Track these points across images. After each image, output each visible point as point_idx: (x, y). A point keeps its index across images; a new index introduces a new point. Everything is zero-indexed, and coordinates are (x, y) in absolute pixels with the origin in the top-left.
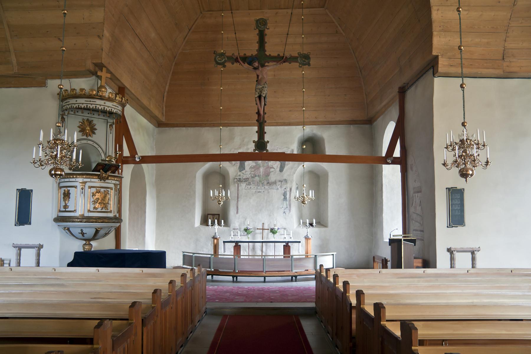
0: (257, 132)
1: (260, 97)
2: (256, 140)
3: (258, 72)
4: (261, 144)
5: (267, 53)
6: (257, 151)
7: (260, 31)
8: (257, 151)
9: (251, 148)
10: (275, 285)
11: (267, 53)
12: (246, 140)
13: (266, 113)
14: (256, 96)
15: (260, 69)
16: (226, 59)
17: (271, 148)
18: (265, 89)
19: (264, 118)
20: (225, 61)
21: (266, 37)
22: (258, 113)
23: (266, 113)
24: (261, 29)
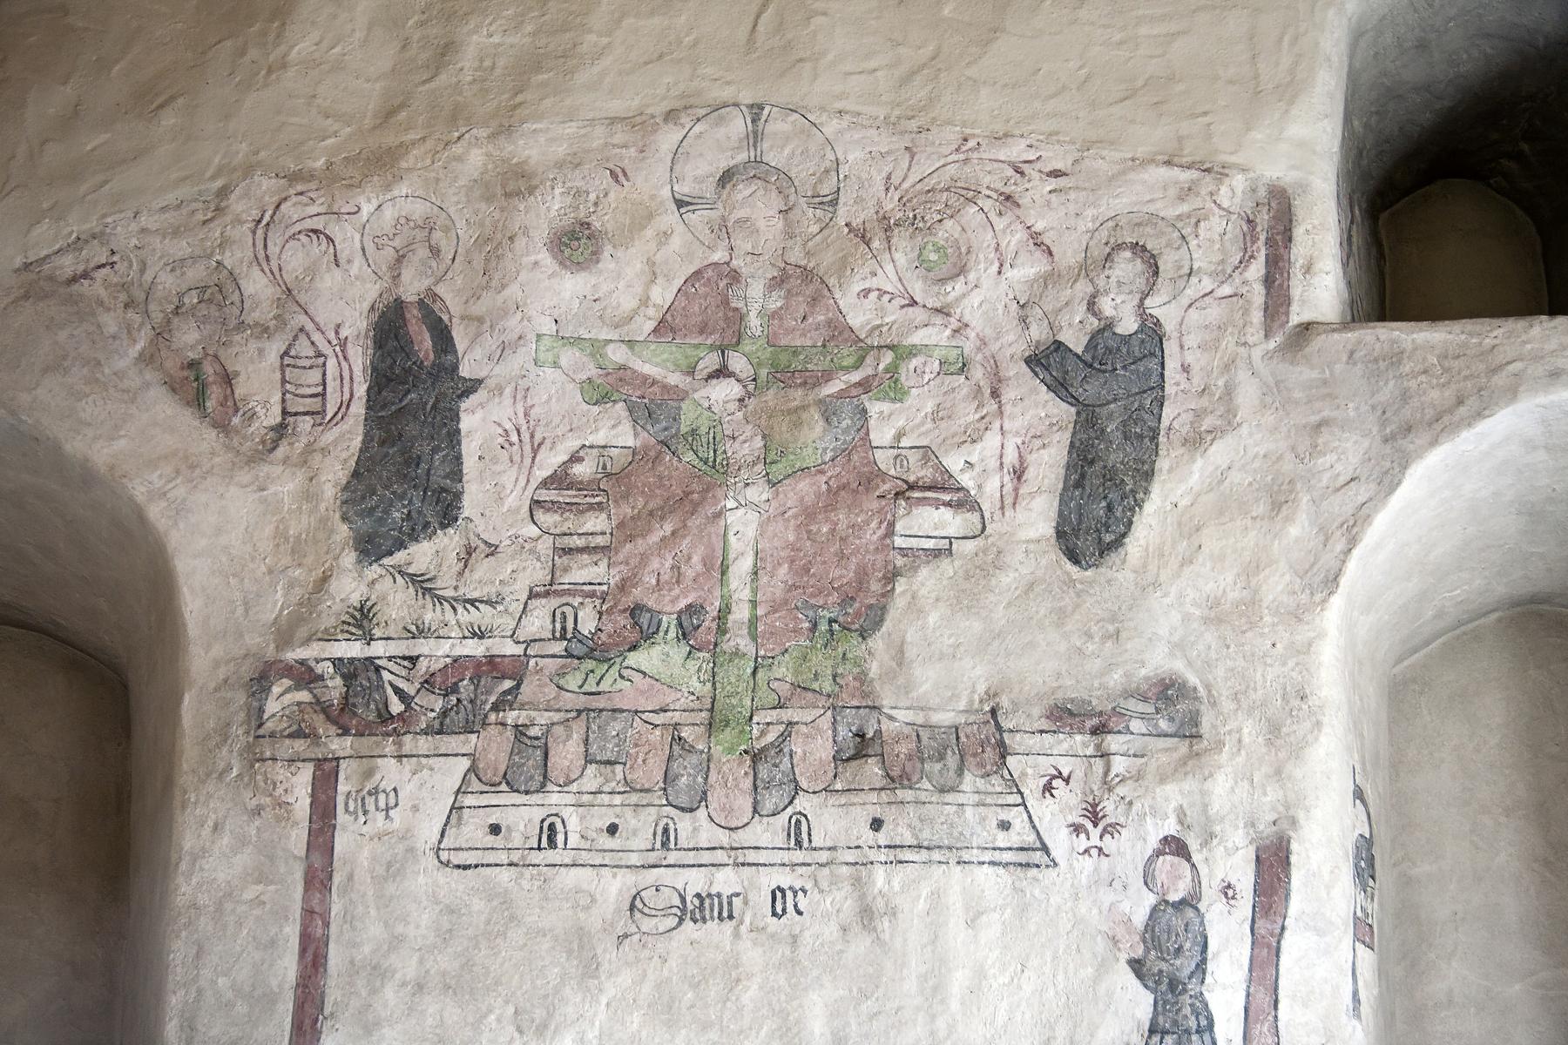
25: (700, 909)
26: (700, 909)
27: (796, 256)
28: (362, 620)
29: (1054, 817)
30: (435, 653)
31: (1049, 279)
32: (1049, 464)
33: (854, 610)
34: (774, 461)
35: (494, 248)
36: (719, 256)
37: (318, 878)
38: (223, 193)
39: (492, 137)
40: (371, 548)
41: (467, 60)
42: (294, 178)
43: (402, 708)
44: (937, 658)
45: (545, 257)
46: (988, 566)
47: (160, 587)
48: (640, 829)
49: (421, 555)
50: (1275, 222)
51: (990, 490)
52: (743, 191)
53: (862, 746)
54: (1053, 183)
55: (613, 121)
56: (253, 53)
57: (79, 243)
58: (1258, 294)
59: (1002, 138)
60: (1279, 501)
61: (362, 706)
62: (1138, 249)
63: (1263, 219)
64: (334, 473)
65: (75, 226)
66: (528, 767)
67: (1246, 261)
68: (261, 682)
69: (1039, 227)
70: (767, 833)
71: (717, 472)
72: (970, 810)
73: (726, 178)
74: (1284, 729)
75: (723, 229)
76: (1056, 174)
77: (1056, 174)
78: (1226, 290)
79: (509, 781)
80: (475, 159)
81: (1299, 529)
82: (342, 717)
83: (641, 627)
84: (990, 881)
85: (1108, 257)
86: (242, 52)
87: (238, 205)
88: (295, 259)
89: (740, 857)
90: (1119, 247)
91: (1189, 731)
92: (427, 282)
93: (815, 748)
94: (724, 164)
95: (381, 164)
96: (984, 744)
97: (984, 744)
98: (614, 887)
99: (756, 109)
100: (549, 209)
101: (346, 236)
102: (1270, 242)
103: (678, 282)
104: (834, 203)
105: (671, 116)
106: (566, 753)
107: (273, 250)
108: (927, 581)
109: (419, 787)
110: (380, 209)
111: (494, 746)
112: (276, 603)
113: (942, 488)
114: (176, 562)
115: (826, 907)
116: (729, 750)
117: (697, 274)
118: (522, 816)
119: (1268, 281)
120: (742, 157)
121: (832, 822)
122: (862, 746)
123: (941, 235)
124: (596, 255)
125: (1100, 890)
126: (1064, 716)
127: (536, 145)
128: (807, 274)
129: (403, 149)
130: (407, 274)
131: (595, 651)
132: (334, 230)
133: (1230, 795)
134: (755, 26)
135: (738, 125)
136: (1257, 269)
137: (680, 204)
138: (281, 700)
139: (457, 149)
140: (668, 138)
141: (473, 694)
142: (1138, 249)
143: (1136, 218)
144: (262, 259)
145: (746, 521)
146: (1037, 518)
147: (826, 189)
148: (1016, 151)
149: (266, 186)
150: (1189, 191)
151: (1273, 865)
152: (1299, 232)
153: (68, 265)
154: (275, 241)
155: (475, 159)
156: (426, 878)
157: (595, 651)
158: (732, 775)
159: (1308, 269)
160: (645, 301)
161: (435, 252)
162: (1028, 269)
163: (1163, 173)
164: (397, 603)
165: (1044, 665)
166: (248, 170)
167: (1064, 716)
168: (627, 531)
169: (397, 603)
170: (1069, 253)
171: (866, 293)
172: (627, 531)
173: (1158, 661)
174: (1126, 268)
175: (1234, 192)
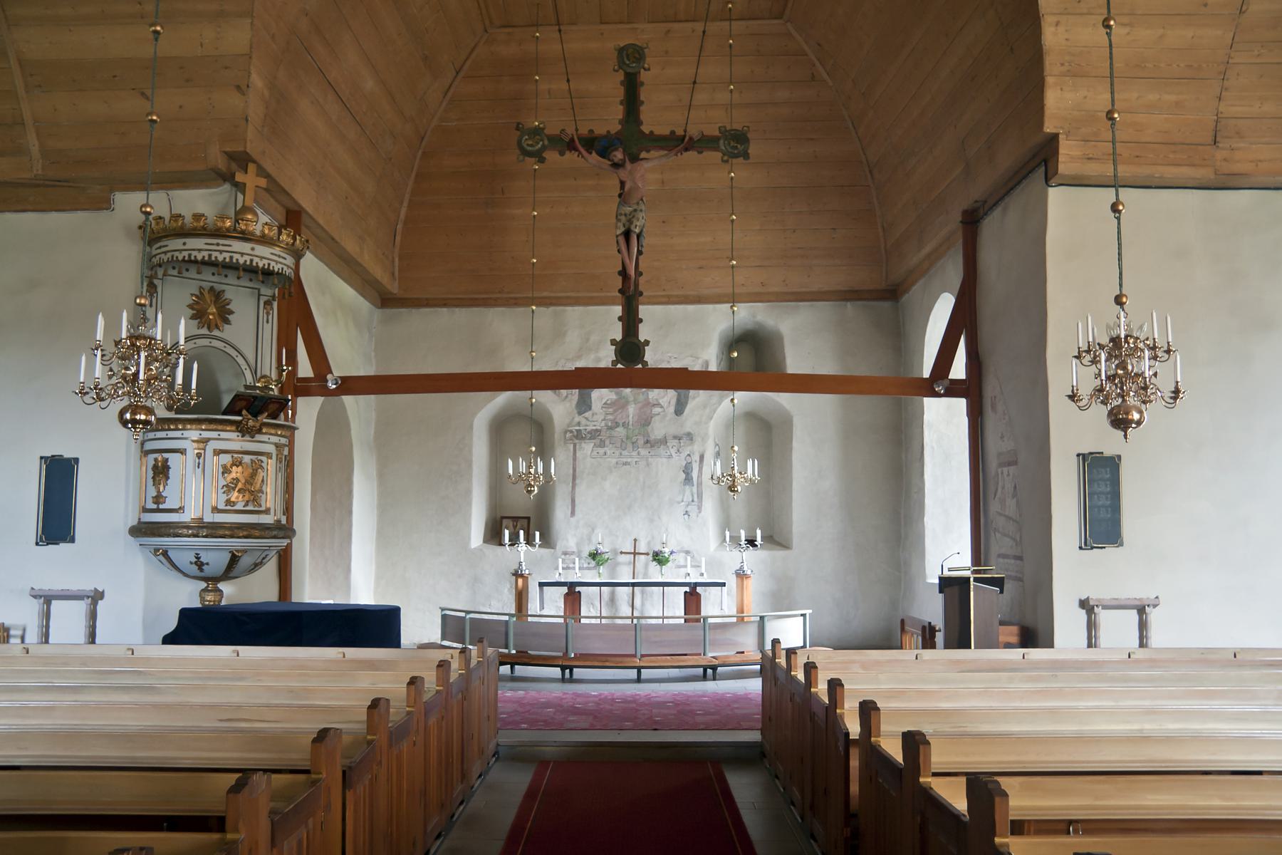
0: (620, 319)
1: (627, 234)
2: (619, 337)
3: (623, 174)
4: (630, 348)
5: (646, 129)
6: (619, 366)
7: (627, 75)
8: (619, 366)
9: (605, 357)
11: (646, 129)
14: (619, 232)
15: (628, 165)
16: (546, 142)
17: (653, 358)
18: (640, 215)
19: (637, 285)
20: (544, 148)
22: (623, 273)
24: (629, 70)
25: (626, 464)
26: (626, 464)
28: (579, 424)
29: (673, 451)
30: (589, 428)
32: (674, 401)
33: (645, 422)
34: (635, 401)
37: (575, 459)
40: (580, 414)
43: (310, 374)
44: (658, 429)
46: (665, 416)
47: (550, 419)
48: (617, 453)
49: (587, 414)
51: (665, 405)
53: (647, 442)
60: (705, 407)
61: (579, 436)
64: (574, 402)
66: (602, 444)
68: (566, 432)
70: (634, 453)
71: (627, 403)
72: (662, 450)
74: (704, 440)
79: (600, 446)
80: (592, 356)
81: (708, 411)
82: (577, 437)
83: (617, 425)
84: (665, 460)
89: (631, 457)
91: (692, 439)
93: (641, 442)
96: (664, 441)
97: (664, 441)
98: (614, 461)
106: (607, 442)
108: (657, 418)
109: (587, 448)
111: (597, 441)
112: (567, 421)
113: (658, 405)
115: (642, 463)
116: (629, 442)
118: (601, 451)
121: (643, 452)
122: (647, 442)
125: (679, 461)
126: (675, 437)
131: (610, 428)
133: (697, 448)
138: (568, 435)
141: (594, 434)
143: (253, 276)
145: (632, 409)
146: (672, 409)
151: (702, 457)
155: (592, 356)
156: (589, 459)
157: (610, 428)
158: (630, 445)
164: (584, 421)
165: (673, 430)
167: (675, 437)
168: (615, 411)
169: (584, 421)
172: (615, 411)
173: (688, 429)
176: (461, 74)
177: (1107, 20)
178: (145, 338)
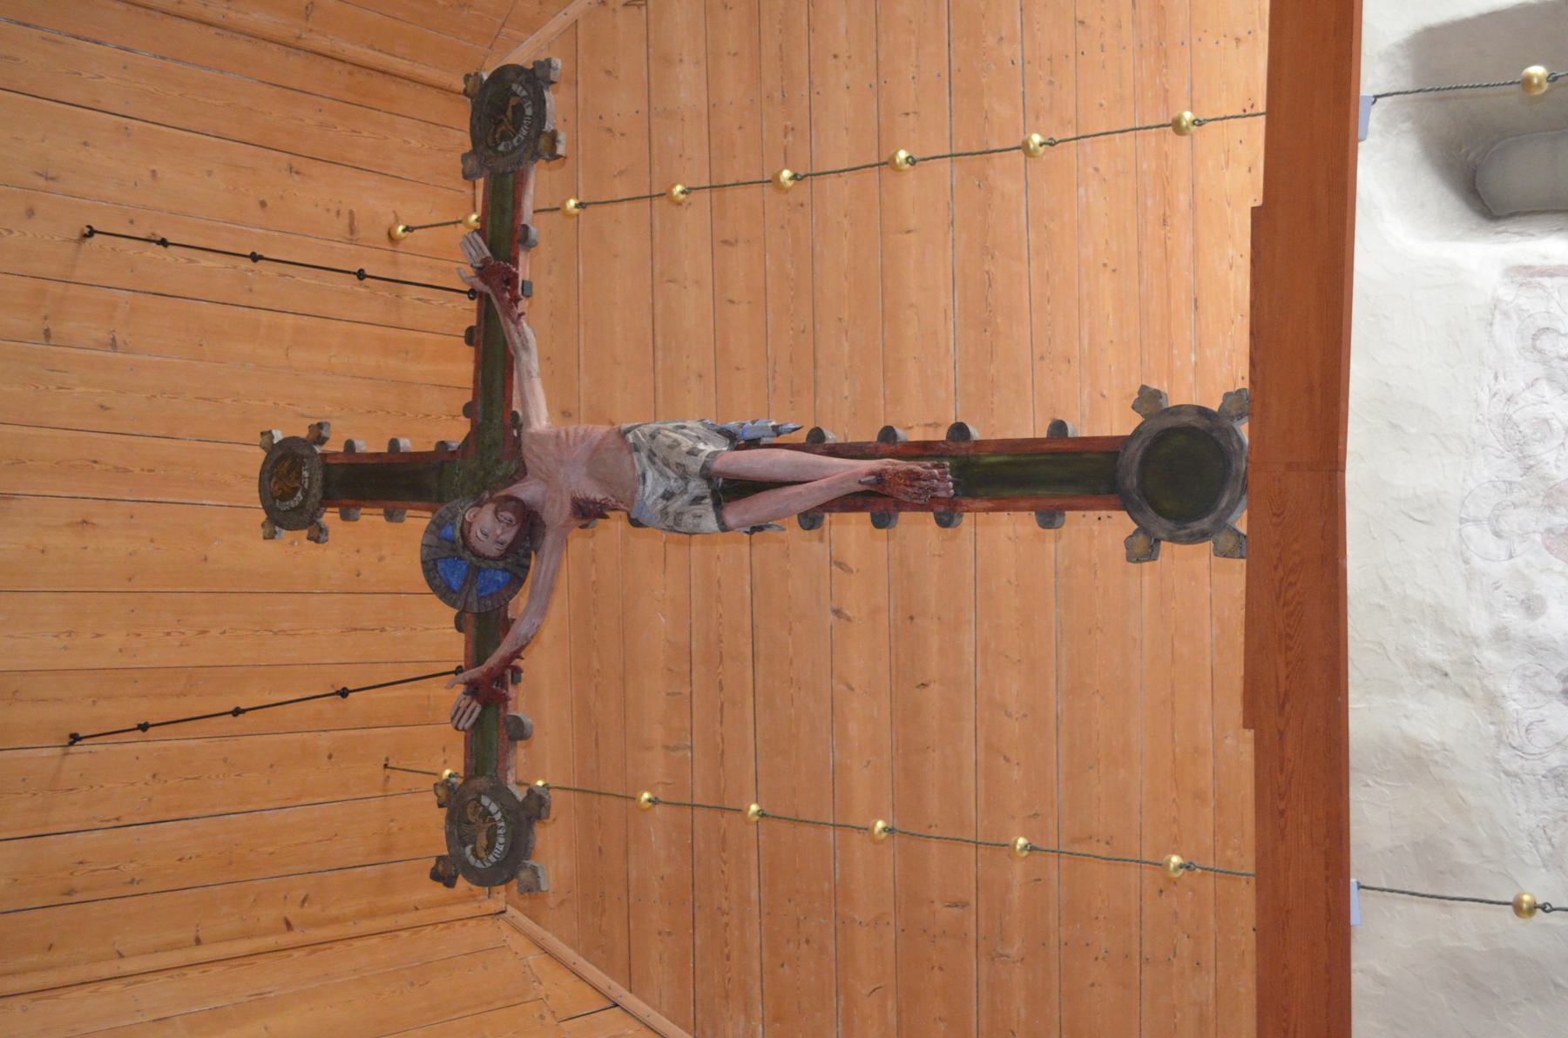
0: (1049, 519)
1: (731, 490)
2: (1116, 526)
3: (556, 513)
4: (1169, 473)
5: (456, 432)
6: (1241, 522)
7: (327, 500)
8: (1241, 522)
9: (1202, 588)
10: (517, 340)
11: (456, 432)
12: (1430, 649)
13: (888, 434)
14: (710, 522)
15: (527, 491)
16: (481, 782)
17: (1210, 363)
18: (669, 434)
19: (923, 450)
20: (499, 791)
21: (1079, 428)
22: (878, 501)
23: (888, 434)
24: (316, 490)
27: (1538, 501)
31: (1551, 379)
35: (1536, 648)
36: (1538, 538)
38: (1507, 773)
39: (1478, 646)
41: (1439, 658)
42: (1500, 741)
45: (1540, 621)
50: (1525, 274)
52: (1504, 527)
54: (1501, 379)
55: (1469, 588)
56: (1437, 757)
57: (1534, 842)
58: (1556, 280)
59: (1478, 403)
62: (1535, 337)
63: (1520, 279)
65: (1525, 843)
67: (1542, 287)
69: (1523, 384)
73: (1498, 534)
75: (1525, 536)
76: (1496, 378)
77: (1496, 378)
78: (1556, 295)
80: (1489, 656)
85: (1540, 351)
86: (1436, 762)
87: (1514, 767)
88: (1539, 742)
90: (1534, 347)
92: (1552, 678)
94: (1490, 536)
95: (1493, 701)
99: (1462, 521)
100: (1514, 619)
101: (1529, 716)
102: (1532, 275)
103: (1552, 558)
104: (1510, 483)
105: (1466, 562)
107: (1536, 751)
110: (1518, 703)
114: (1360, 145)
117: (1548, 548)
119: (1551, 275)
120: (1487, 527)
123: (1528, 431)
124: (1539, 597)
127: (1480, 623)
128: (1548, 496)
129: (1484, 689)
130: (1549, 687)
132: (1526, 722)
134: (815, 361)
135: (1470, 529)
136: (1546, 281)
137: (1511, 557)
139: (1484, 663)
140: (1478, 563)
142: (1535, 337)
144: (1541, 756)
147: (1503, 487)
148: (1484, 397)
149: (1503, 754)
150: (1506, 314)
152: (1527, 263)
153: (1545, 848)
154: (1530, 749)
159: (1546, 258)
160: (1562, 574)
161: (1537, 674)
162: (1545, 389)
163: (1496, 327)
166: (1496, 761)
170: (1538, 370)
171: (1557, 467)
174: (1545, 343)
175: (1507, 294)
176: (619, 992)
177: (1517, 907)
178: (1540, 690)
